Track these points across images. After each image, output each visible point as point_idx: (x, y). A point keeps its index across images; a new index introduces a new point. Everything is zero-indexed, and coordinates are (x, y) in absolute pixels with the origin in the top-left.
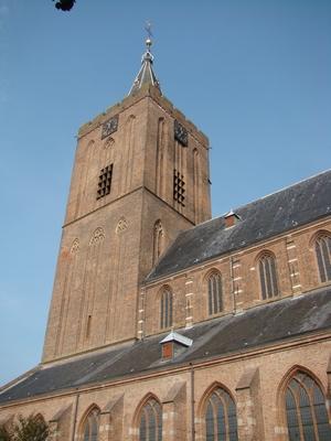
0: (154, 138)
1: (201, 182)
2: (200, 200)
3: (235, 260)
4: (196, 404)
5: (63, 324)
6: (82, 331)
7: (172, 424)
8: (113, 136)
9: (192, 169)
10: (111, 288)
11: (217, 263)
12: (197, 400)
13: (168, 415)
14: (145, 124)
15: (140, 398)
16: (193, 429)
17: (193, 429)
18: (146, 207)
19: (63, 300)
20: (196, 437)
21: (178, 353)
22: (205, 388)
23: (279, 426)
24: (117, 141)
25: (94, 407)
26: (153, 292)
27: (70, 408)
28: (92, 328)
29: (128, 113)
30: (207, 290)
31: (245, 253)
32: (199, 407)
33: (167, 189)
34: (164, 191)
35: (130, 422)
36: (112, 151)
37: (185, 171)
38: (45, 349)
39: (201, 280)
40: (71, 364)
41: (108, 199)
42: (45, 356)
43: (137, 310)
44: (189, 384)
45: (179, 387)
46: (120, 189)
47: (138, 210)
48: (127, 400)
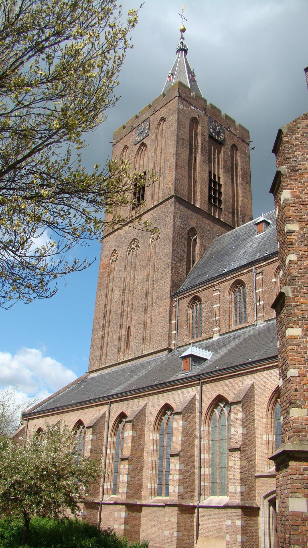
0: (187, 143)
1: (240, 180)
2: (240, 200)
3: (258, 271)
4: (203, 414)
5: (106, 335)
7: (181, 431)
8: (145, 141)
9: (231, 169)
10: (147, 299)
11: (199, 292)
13: (177, 423)
14: (175, 127)
16: (200, 435)
18: (178, 215)
19: (105, 312)
23: (268, 434)
24: (149, 147)
25: (167, 408)
26: (185, 303)
28: (132, 338)
29: (159, 115)
30: (233, 301)
33: (202, 194)
34: (198, 197)
36: (146, 156)
37: (221, 171)
38: (91, 359)
39: (227, 292)
40: (113, 372)
42: (91, 365)
43: (170, 320)
44: (198, 397)
47: (170, 220)
48: (149, 409)
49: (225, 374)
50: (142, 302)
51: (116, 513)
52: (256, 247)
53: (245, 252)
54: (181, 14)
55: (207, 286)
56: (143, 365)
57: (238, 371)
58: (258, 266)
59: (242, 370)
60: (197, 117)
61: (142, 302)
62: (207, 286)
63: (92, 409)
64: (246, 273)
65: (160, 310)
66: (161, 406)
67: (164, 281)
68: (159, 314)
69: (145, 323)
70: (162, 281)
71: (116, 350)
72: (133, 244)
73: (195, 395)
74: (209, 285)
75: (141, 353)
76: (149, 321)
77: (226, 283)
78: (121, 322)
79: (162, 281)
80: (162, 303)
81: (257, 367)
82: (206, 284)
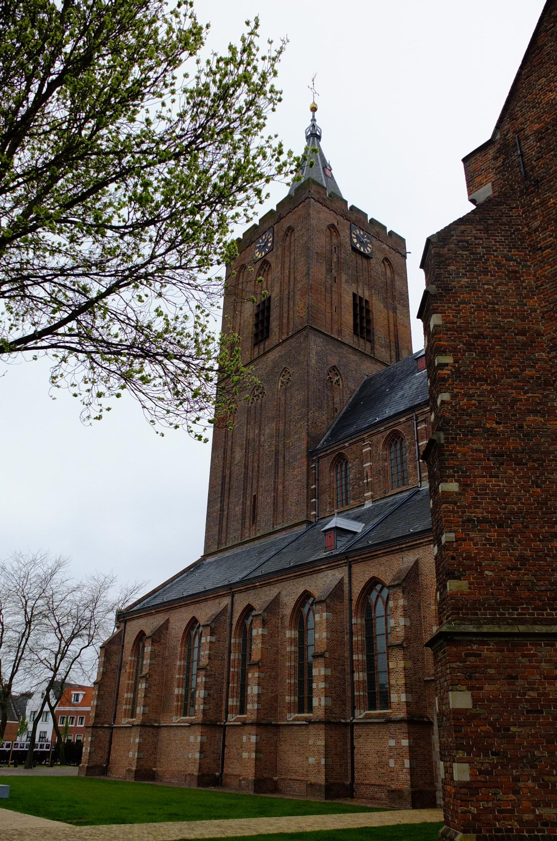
5: (225, 507)
6: (248, 515)
7: (325, 625)
10: (277, 460)
11: (344, 447)
12: (355, 597)
15: (296, 598)
17: (351, 630)
19: (224, 477)
20: (355, 639)
21: (342, 545)
22: (363, 584)
25: (306, 595)
27: (341, 583)
32: (357, 604)
35: (287, 623)
41: (268, 344)
44: (346, 580)
45: (336, 583)
46: (281, 332)
49: (380, 550)
51: (244, 738)
52: (417, 388)
53: (403, 395)
54: (311, 86)
55: (354, 440)
57: (396, 546)
58: (420, 412)
59: (402, 544)
60: (336, 224)
62: (354, 440)
63: (210, 603)
65: (295, 473)
66: (299, 595)
68: (294, 478)
69: (276, 489)
70: (297, 436)
71: (239, 526)
74: (357, 439)
75: (271, 528)
76: (280, 487)
77: (379, 436)
78: (245, 489)
79: (297, 436)
80: (296, 464)
81: (420, 539)
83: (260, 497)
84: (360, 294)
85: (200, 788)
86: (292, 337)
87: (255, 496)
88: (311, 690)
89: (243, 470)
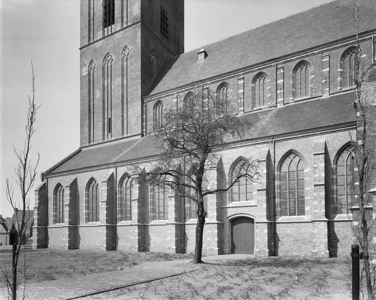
31: (212, 83)
40: (111, 146)
50: (119, 101)
56: (130, 143)
61: (119, 101)
64: (317, 54)
67: (135, 88)
72: (108, 57)
73: (113, 172)
75: (121, 136)
78: (104, 114)
82: (158, 95)
83: (113, 120)
84: (163, 7)
85: (40, 249)
86: (130, 26)
87: (110, 118)
88: (275, 211)
89: (102, 103)
